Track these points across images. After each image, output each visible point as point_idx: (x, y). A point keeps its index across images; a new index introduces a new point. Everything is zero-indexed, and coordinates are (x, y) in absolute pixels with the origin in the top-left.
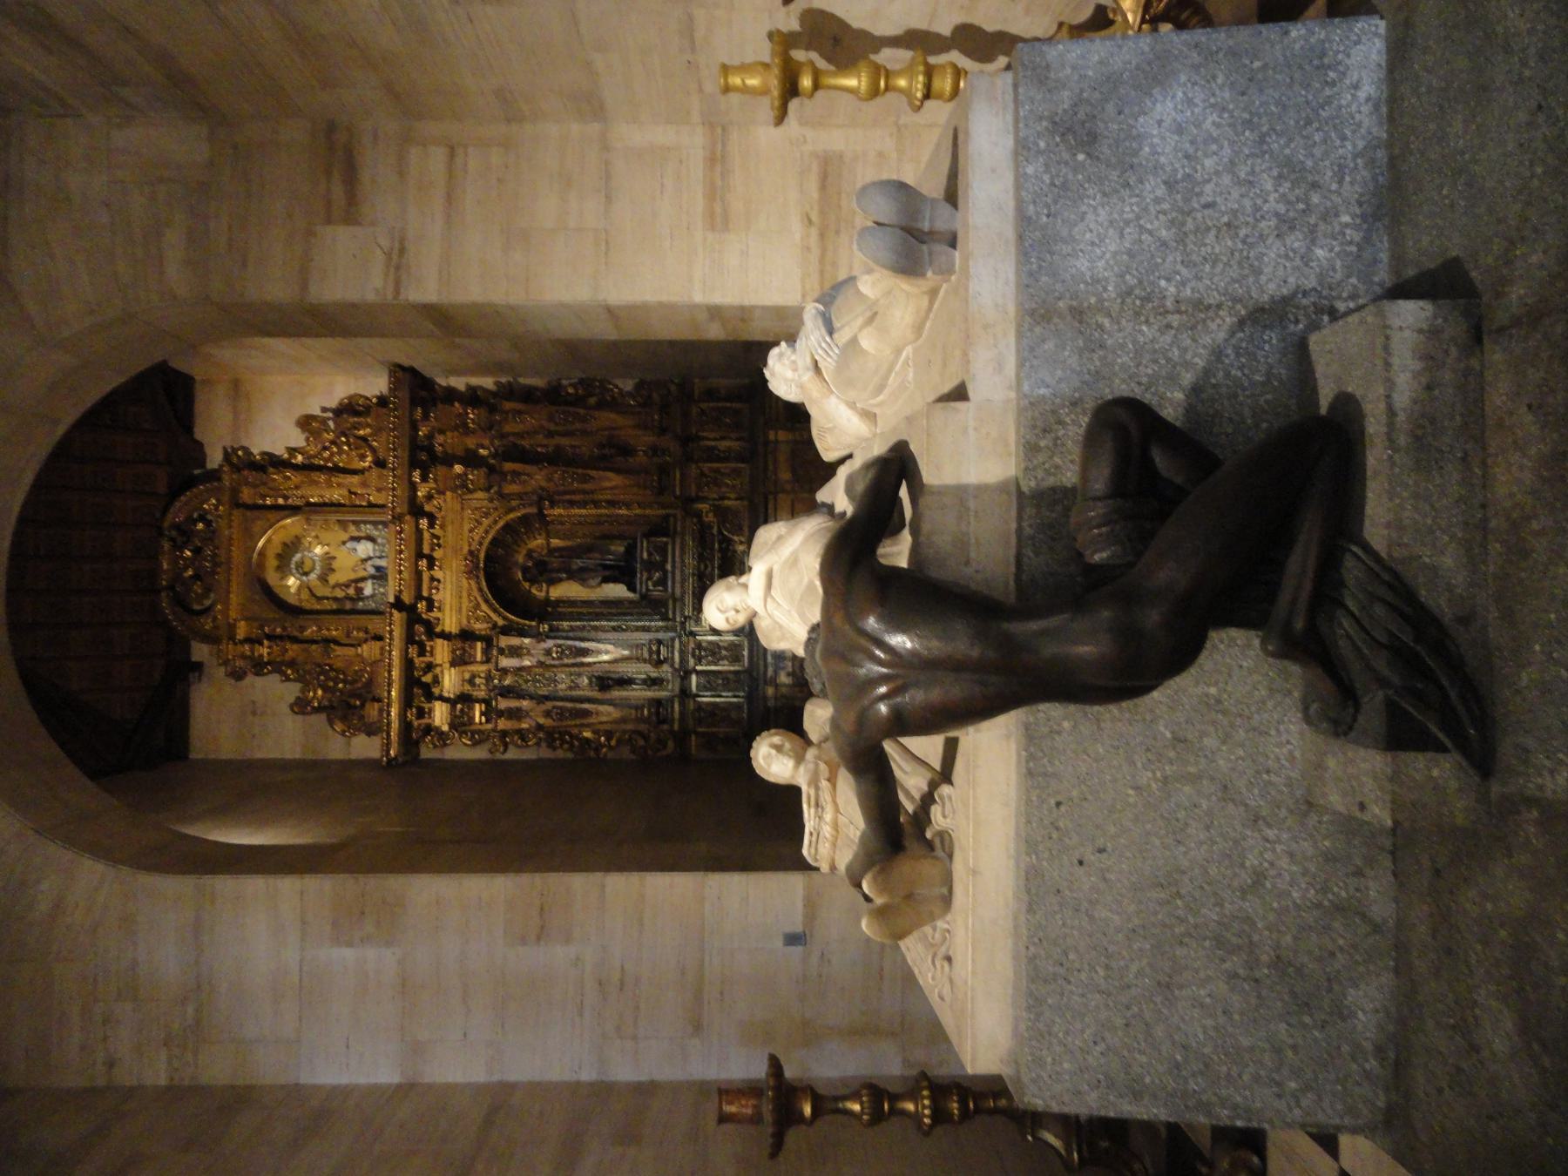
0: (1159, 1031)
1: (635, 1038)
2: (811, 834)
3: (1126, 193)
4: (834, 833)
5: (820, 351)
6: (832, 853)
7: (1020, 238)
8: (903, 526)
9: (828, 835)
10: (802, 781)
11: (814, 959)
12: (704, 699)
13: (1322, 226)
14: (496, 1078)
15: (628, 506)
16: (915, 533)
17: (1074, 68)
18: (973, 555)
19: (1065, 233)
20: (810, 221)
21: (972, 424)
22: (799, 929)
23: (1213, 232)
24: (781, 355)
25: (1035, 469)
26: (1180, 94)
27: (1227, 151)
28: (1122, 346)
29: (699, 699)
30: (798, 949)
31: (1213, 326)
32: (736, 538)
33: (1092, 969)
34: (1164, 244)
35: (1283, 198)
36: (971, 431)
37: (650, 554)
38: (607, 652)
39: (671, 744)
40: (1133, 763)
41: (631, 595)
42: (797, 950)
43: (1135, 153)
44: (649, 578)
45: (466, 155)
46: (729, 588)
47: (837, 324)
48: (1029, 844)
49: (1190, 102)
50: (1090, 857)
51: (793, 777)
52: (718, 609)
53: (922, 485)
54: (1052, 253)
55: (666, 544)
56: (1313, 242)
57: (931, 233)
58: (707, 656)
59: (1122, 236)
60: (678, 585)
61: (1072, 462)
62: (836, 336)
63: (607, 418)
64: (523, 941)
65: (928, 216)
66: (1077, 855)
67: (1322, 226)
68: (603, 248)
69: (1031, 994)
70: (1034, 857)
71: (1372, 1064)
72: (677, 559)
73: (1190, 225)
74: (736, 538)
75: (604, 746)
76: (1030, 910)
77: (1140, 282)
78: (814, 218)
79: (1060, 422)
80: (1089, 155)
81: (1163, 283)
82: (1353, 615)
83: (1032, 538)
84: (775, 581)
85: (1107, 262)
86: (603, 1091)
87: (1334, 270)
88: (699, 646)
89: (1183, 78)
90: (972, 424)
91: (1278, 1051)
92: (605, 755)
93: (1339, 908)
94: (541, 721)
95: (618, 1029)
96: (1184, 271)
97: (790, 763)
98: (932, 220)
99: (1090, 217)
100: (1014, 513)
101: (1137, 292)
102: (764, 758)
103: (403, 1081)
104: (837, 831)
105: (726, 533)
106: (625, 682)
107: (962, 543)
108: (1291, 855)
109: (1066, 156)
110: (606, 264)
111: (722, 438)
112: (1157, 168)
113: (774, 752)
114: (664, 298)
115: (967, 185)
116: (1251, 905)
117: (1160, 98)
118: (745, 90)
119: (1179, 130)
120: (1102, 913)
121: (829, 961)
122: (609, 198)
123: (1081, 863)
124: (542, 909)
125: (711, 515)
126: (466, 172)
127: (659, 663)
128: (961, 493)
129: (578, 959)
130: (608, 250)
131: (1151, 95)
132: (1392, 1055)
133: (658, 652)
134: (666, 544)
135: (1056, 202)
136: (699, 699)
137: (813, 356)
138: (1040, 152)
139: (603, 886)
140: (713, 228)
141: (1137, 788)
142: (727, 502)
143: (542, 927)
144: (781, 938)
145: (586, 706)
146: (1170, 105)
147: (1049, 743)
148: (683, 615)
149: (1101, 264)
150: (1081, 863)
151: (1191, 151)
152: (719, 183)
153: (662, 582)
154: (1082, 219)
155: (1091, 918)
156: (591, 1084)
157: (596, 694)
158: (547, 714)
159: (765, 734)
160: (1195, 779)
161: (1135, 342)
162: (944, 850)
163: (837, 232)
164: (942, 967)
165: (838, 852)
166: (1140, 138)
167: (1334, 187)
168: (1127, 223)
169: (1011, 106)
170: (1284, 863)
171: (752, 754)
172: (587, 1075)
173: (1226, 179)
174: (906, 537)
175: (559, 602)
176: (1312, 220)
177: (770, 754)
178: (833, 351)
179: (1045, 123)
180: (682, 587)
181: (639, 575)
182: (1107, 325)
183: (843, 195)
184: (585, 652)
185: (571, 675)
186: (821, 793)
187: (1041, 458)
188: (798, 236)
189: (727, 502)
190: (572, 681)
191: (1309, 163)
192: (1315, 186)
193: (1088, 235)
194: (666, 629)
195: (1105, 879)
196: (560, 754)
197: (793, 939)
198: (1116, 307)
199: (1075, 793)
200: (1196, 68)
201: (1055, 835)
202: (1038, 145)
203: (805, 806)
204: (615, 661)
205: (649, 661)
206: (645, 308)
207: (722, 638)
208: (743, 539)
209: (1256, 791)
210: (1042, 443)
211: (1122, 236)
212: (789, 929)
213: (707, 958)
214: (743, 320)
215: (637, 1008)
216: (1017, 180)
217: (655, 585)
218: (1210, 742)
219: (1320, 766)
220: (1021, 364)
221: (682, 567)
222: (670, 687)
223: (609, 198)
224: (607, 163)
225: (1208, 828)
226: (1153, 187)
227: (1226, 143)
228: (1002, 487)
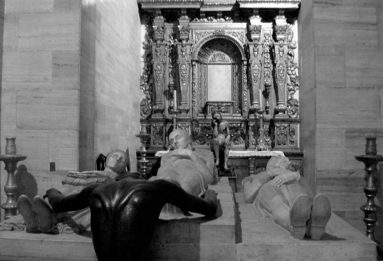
1: (17, 103)
4: (76, 184)
5: (278, 179)
8: (187, 214)
11: (45, 175)
14: (4, 50)
16: (182, 220)
18: (170, 244)
36: (223, 244)
45: (374, 30)
47: (289, 186)
53: (199, 223)
57: (310, 227)
62: (284, 186)
64: (54, 58)
65: (318, 226)
95: (20, 96)
97: (113, 165)
98: (316, 227)
103: (5, 15)
107: (176, 239)
113: (118, 159)
121: (44, 181)
122: (359, 88)
124: (66, 65)
126: (367, 30)
128: (196, 240)
129: (47, 80)
130: (337, 88)
137: (277, 175)
139: (74, 89)
140: (348, 132)
144: (53, 161)
163: (347, 185)
164: (10, 227)
165: (69, 185)
174: (181, 216)
178: (278, 184)
188: (345, 168)
215: (28, 103)
223: (359, 88)
224: (373, 88)
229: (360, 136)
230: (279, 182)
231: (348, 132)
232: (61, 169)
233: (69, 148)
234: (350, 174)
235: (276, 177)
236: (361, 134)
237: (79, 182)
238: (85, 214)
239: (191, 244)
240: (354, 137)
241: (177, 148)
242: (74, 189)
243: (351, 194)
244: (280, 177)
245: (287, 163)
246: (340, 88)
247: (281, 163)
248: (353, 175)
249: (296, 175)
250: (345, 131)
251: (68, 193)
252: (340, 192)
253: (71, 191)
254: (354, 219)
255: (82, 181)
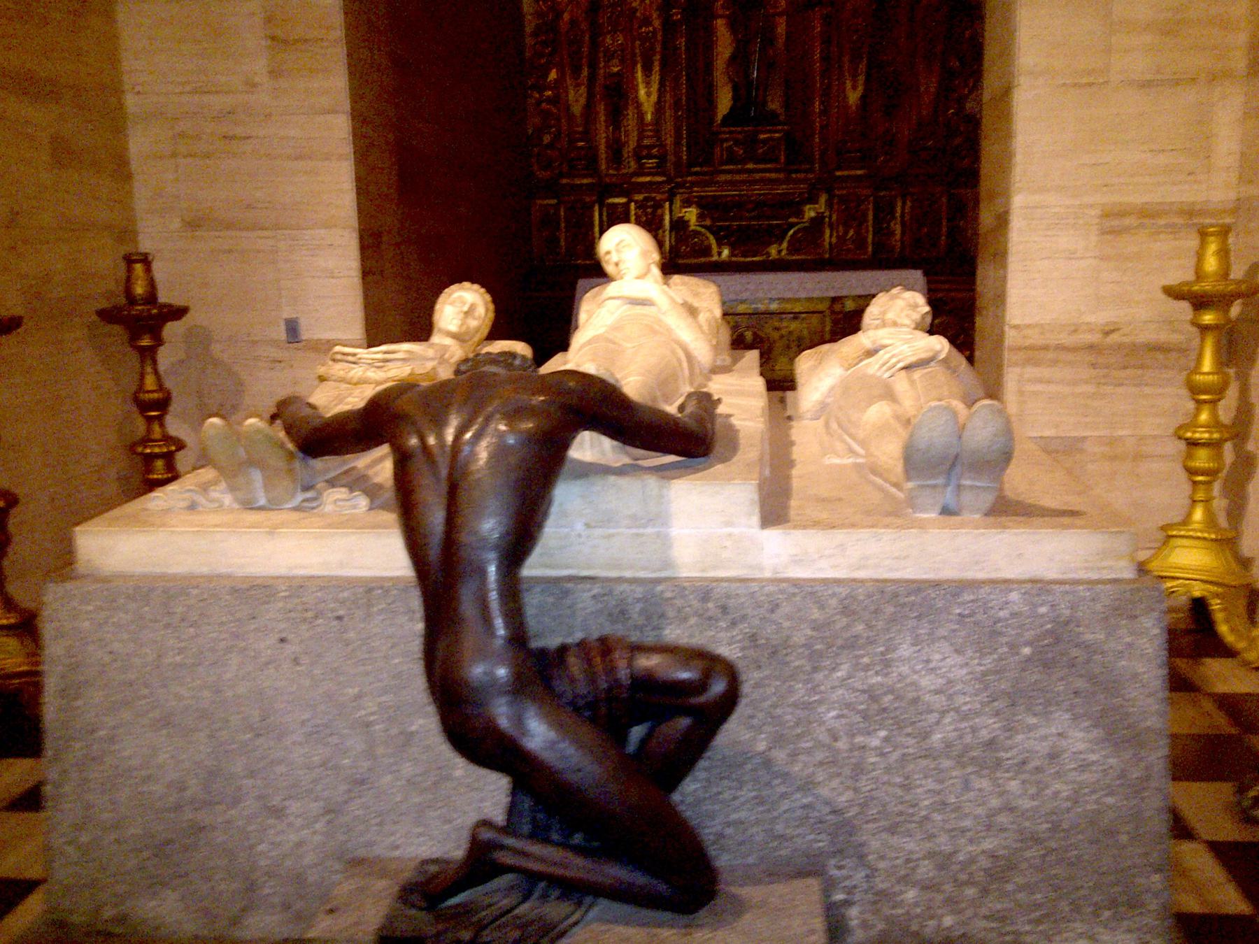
0: (126, 715)
2: (354, 355)
3: (983, 697)
5: (887, 356)
6: (333, 378)
7: (936, 584)
9: (352, 373)
10: (436, 339)
11: (274, 353)
12: (597, 215)
13: (939, 897)
15: (824, 112)
17: (1130, 645)
19: (943, 632)
20: (1107, 333)
21: (735, 531)
22: (305, 335)
23: (938, 787)
24: (915, 306)
25: (683, 597)
26: (1093, 757)
27: (1026, 804)
28: (814, 690)
29: (597, 208)
30: (283, 335)
31: (835, 783)
32: (785, 245)
33: (181, 651)
34: (926, 735)
35: (972, 860)
37: (765, 141)
38: (648, 94)
39: (542, 174)
40: (385, 691)
41: (719, 117)
42: (281, 333)
43: (1029, 709)
44: (737, 143)
46: (645, 254)
47: (917, 374)
48: (298, 586)
49: (1084, 767)
50: (290, 649)
51: (440, 330)
52: (621, 241)
54: (919, 618)
55: (776, 160)
56: (926, 888)
58: (646, 215)
59: (937, 692)
60: (729, 177)
61: (691, 636)
62: (903, 373)
63: (929, 86)
66: (291, 637)
67: (939, 897)
68: (1085, 80)
69: (152, 590)
70: (287, 594)
71: (108, 913)
72: (757, 176)
73: (947, 763)
74: (785, 245)
75: (541, 95)
76: (234, 591)
77: (885, 710)
78: (1114, 338)
79: (734, 623)
80: (1029, 660)
81: (883, 733)
82: (513, 909)
83: (610, 593)
84: (639, 310)
85: (907, 676)
86: (116, 122)
87: (894, 908)
88: (659, 205)
89: (1112, 761)
90: (735, 531)
91: (116, 826)
92: (531, 96)
93: (251, 887)
94: (566, 16)
95: (182, 135)
96: (895, 756)
99: (959, 659)
100: (642, 574)
101: (875, 706)
102: (460, 297)
104: (355, 384)
105: (791, 232)
106: (616, 117)
108: (299, 844)
109: (1029, 635)
110: (1064, 84)
111: (903, 224)
112: (1009, 729)
113: (465, 309)
114: (1019, 158)
115: (1005, 527)
116: (250, 805)
117: (1091, 736)
118: (1200, 257)
119: (1053, 756)
120: (235, 660)
123: (282, 640)
125: (813, 214)
127: (638, 157)
128: (660, 518)
131: (1095, 726)
132: (118, 930)
133: (650, 157)
134: (776, 160)
135: (976, 623)
136: (597, 208)
137: (885, 346)
138: (1035, 606)
139: (334, 112)
141: (359, 697)
142: (828, 232)
143: (285, 42)
145: (585, 73)
146: (1081, 746)
147: (402, 610)
148: (693, 184)
149: (905, 669)
150: (282, 640)
151: (1030, 766)
152: (1162, 222)
153: (732, 159)
154: (957, 651)
155: (229, 650)
156: (121, 106)
157: (601, 80)
158: (574, 22)
159: (488, 297)
160: (370, 754)
161: (820, 702)
162: (304, 501)
163: (1094, 366)
166: (1046, 715)
167: (984, 911)
168: (950, 697)
169: (1094, 576)
170: (294, 838)
171: (467, 284)
172: (130, 101)
173: (995, 802)
175: (710, 31)
176: (948, 888)
177: (464, 303)
178: (887, 370)
179: (1067, 612)
180: (726, 182)
181: (739, 129)
182: (839, 674)
183: (1140, 372)
184: (647, 70)
185: (622, 51)
186: (399, 364)
187: (695, 604)
188: (1090, 318)
189: (828, 232)
190: (615, 52)
191: (1009, 887)
192: (985, 892)
193: (937, 657)
194: (678, 164)
195: (267, 664)
196: (529, 41)
197: (292, 329)
198: (858, 685)
199: (352, 635)
200: (1123, 775)
201: (310, 614)
202: (1042, 605)
203: (384, 348)
204: (638, 105)
205: (639, 147)
206: (1008, 135)
207: (667, 233)
208: (784, 253)
209: (360, 812)
210: (710, 605)
211: (937, 692)
212: (303, 323)
213: (266, 233)
214: (995, 255)
216: (1006, 581)
217: (729, 149)
218: (408, 769)
219: (383, 874)
220: (796, 583)
221: (749, 181)
222: (611, 172)
223: (1145, 85)
225: (323, 764)
226: (989, 726)
227: (1035, 803)
228: (668, 564)
229: (1142, 226)
230: (888, 365)
231: (1107, 214)
232: (316, 337)
233: (333, 277)
234: (1107, 333)
235: (881, 352)
236: (1146, 221)
237: (364, 376)
238: (381, 459)
239: (649, 530)
240: (1126, 230)
241: (622, 278)
242: (350, 395)
243: (1109, 389)
244: (894, 352)
245: (919, 309)
246: (1091, 85)
247: (902, 310)
248: (1114, 338)
249: (939, 344)
250: (1098, 212)
251: (336, 405)
252: (1075, 383)
253: (340, 400)
254: (1113, 458)
255: (372, 374)
